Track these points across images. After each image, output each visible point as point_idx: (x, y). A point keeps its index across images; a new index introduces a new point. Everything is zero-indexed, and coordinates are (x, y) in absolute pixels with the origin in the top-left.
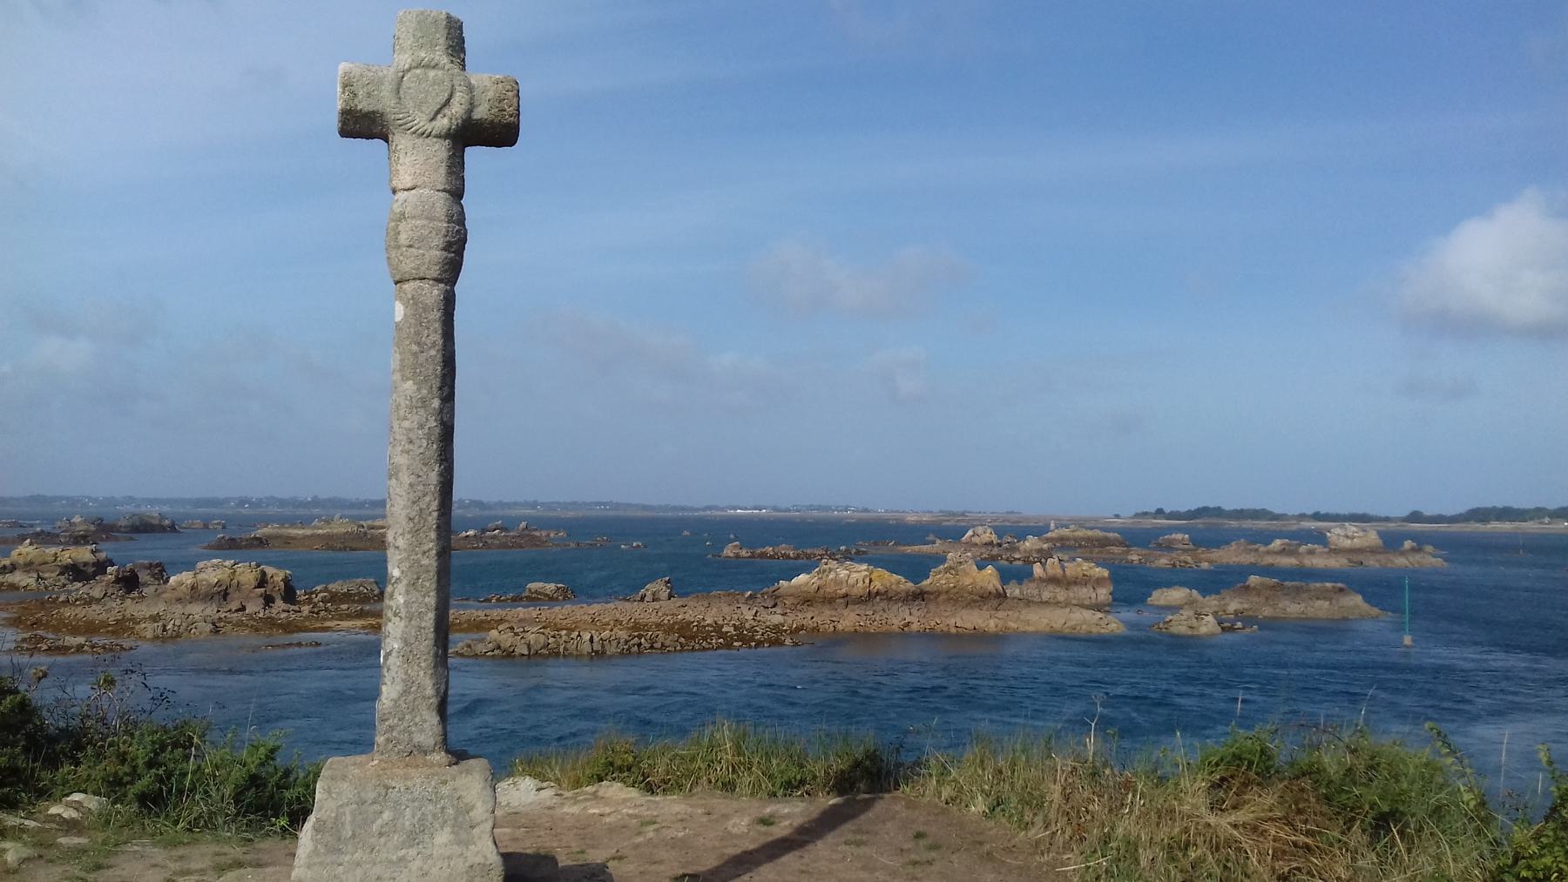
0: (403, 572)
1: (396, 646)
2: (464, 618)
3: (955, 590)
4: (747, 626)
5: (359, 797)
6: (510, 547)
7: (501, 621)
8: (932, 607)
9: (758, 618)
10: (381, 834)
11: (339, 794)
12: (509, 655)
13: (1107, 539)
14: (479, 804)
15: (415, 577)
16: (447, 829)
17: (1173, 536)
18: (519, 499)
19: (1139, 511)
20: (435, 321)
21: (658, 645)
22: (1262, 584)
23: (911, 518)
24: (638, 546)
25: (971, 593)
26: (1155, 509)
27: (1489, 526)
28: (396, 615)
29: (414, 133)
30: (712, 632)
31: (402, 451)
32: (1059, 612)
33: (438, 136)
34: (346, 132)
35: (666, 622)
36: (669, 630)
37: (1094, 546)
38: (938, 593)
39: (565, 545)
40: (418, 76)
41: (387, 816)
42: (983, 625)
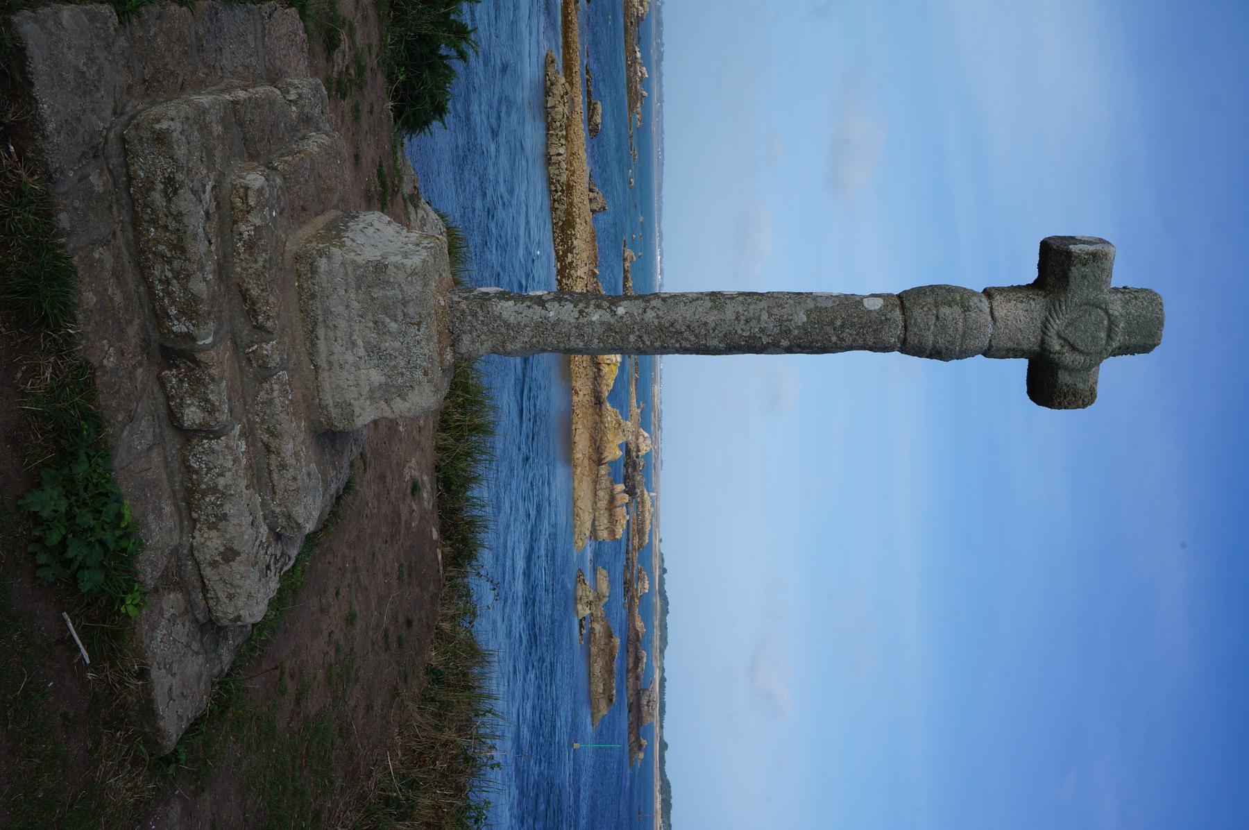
0: (622, 317)
1: (551, 314)
2: (574, 56)
3: (603, 428)
4: (572, 272)
5: (409, 301)
6: (628, 85)
7: (572, 84)
8: (591, 410)
9: (578, 280)
10: (376, 322)
11: (411, 283)
12: (547, 92)
13: (644, 534)
14: (408, 405)
15: (617, 330)
16: (383, 380)
17: (647, 582)
18: (664, 89)
19: (664, 556)
20: (865, 340)
21: (556, 205)
22: (614, 646)
23: (656, 389)
24: (631, 183)
25: (601, 439)
26: (667, 568)
27: (658, 794)
28: (581, 312)
29: (1047, 319)
30: (567, 245)
31: (738, 312)
32: (590, 504)
33: (1043, 342)
34: (1046, 247)
35: (574, 209)
36: (568, 213)
37: (638, 528)
38: (601, 416)
39: (630, 127)
40: (1102, 323)
41: (393, 326)
42: (578, 449)
